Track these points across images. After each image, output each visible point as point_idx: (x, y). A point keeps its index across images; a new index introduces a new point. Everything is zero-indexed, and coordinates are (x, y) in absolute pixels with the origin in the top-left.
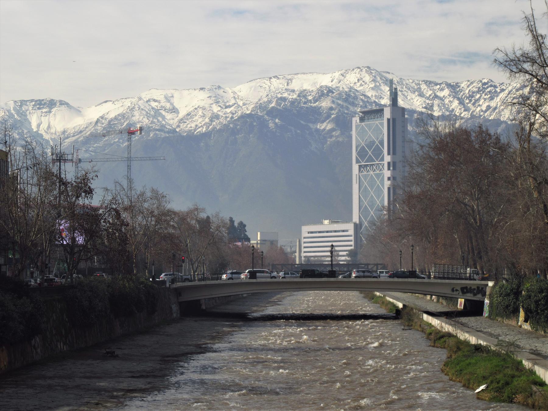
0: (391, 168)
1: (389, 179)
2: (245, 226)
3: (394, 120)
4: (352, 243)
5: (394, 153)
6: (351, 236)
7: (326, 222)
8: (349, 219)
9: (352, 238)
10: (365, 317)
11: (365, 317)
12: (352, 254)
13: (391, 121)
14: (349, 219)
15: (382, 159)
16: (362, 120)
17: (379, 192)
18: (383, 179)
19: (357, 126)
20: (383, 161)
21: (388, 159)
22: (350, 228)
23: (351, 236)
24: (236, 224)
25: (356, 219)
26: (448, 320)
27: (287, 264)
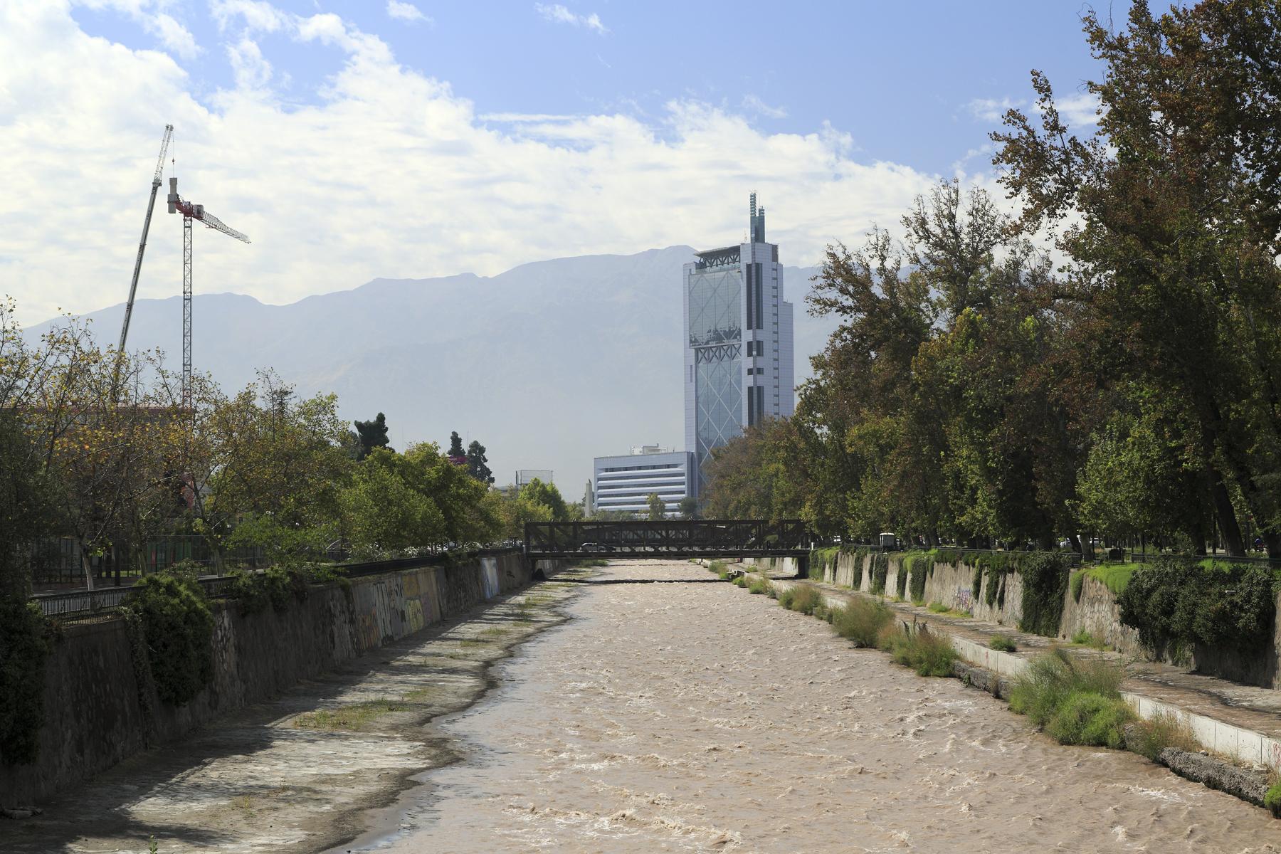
0: (754, 353)
1: (750, 372)
2: (482, 450)
12: (688, 506)
13: (754, 345)
24: (465, 446)
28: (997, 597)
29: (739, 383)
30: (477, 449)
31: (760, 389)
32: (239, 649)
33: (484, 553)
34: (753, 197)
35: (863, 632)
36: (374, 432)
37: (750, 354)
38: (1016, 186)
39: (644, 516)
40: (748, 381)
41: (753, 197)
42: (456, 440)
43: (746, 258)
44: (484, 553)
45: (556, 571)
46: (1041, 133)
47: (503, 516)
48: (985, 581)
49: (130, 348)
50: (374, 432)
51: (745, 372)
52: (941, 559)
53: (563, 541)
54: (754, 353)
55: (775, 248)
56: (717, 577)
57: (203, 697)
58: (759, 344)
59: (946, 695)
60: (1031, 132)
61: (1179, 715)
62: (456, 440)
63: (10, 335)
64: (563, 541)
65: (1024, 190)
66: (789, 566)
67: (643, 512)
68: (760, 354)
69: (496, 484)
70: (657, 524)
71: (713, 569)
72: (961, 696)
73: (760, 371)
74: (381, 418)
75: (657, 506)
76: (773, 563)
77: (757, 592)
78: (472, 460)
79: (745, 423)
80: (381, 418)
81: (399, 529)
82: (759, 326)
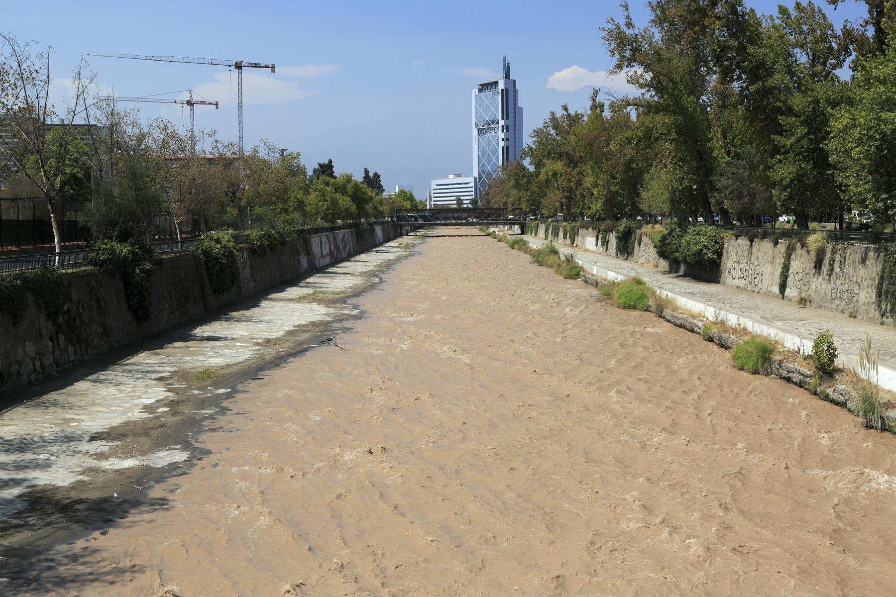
1: (503, 139)
2: (379, 176)
3: (507, 90)
4: (473, 193)
5: (507, 118)
7: (451, 176)
8: (470, 174)
9: (473, 189)
10: (240, 89)
11: (240, 89)
12: (474, 202)
14: (470, 174)
15: (497, 123)
16: (480, 90)
17: (495, 152)
19: (476, 96)
21: (502, 123)
22: (471, 180)
24: (371, 175)
25: (476, 174)
26: (33, 403)
27: (416, 207)
28: (605, 243)
29: (498, 145)
30: (377, 176)
32: (252, 268)
33: (376, 223)
34: (505, 59)
35: (539, 258)
36: (326, 169)
38: (613, 52)
39: (454, 206)
41: (505, 59)
42: (366, 172)
43: (501, 86)
44: (376, 223)
45: (412, 231)
46: (624, 28)
47: (385, 209)
48: (600, 236)
49: (196, 129)
50: (326, 169)
52: (582, 227)
53: (413, 218)
55: (514, 81)
56: (484, 234)
57: (234, 289)
58: (507, 126)
59: (575, 288)
60: (618, 28)
61: (670, 295)
62: (366, 172)
63: (30, 125)
64: (413, 218)
65: (617, 54)
66: (517, 229)
67: (453, 204)
69: (385, 194)
70: (460, 210)
71: (481, 230)
72: (580, 287)
74: (330, 161)
75: (459, 201)
76: (510, 228)
77: (500, 241)
78: (373, 181)
79: (501, 163)
80: (330, 161)
81: (332, 214)
82: (507, 118)
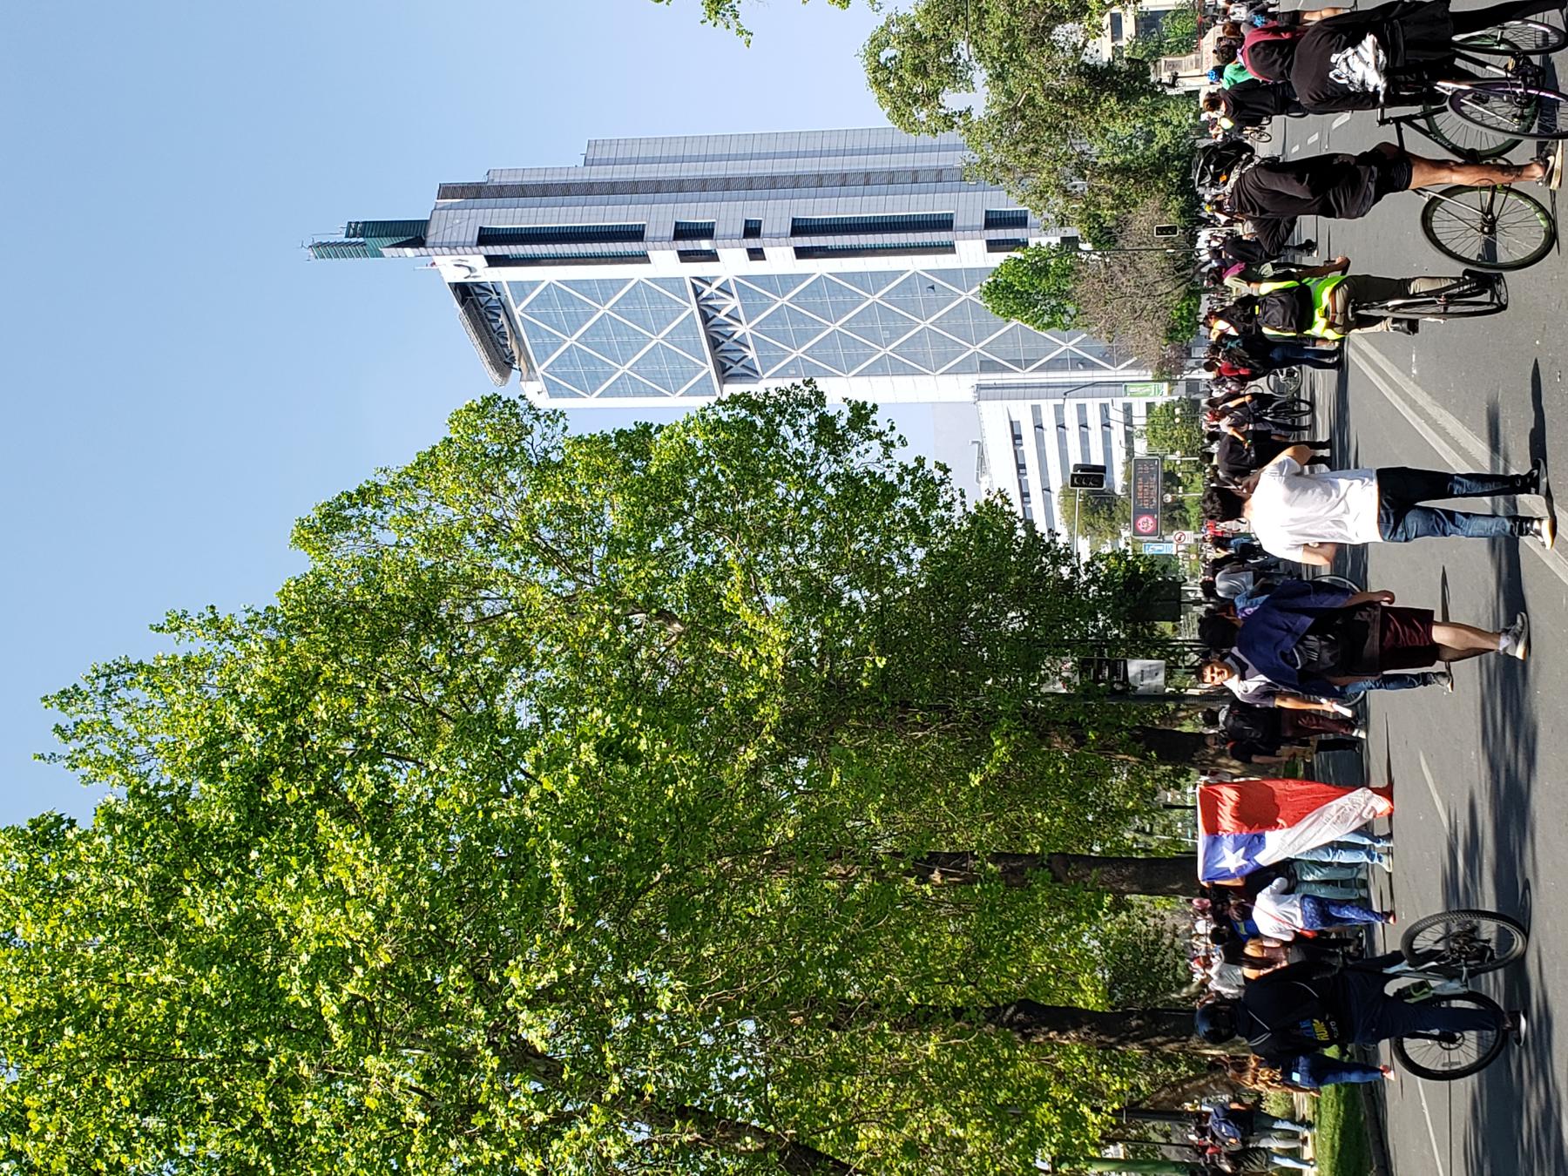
0: (705, 245)
1: (756, 254)
6: (1036, 410)
15: (675, 283)
18: (766, 281)
20: (680, 280)
23: (1036, 410)
31: (799, 228)
37: (711, 256)
40: (780, 258)
51: (757, 268)
54: (705, 245)
58: (683, 232)
68: (706, 232)
73: (752, 230)
